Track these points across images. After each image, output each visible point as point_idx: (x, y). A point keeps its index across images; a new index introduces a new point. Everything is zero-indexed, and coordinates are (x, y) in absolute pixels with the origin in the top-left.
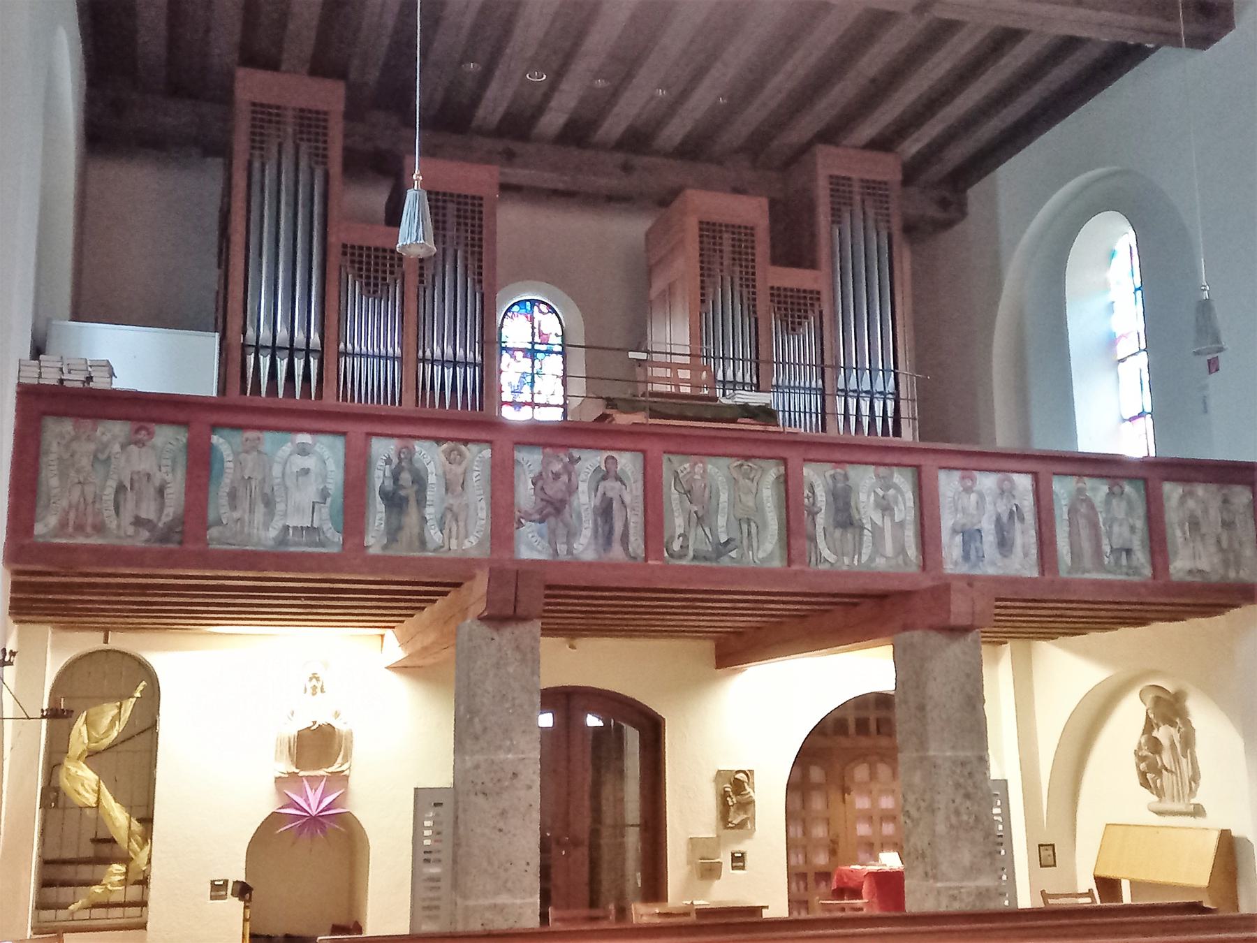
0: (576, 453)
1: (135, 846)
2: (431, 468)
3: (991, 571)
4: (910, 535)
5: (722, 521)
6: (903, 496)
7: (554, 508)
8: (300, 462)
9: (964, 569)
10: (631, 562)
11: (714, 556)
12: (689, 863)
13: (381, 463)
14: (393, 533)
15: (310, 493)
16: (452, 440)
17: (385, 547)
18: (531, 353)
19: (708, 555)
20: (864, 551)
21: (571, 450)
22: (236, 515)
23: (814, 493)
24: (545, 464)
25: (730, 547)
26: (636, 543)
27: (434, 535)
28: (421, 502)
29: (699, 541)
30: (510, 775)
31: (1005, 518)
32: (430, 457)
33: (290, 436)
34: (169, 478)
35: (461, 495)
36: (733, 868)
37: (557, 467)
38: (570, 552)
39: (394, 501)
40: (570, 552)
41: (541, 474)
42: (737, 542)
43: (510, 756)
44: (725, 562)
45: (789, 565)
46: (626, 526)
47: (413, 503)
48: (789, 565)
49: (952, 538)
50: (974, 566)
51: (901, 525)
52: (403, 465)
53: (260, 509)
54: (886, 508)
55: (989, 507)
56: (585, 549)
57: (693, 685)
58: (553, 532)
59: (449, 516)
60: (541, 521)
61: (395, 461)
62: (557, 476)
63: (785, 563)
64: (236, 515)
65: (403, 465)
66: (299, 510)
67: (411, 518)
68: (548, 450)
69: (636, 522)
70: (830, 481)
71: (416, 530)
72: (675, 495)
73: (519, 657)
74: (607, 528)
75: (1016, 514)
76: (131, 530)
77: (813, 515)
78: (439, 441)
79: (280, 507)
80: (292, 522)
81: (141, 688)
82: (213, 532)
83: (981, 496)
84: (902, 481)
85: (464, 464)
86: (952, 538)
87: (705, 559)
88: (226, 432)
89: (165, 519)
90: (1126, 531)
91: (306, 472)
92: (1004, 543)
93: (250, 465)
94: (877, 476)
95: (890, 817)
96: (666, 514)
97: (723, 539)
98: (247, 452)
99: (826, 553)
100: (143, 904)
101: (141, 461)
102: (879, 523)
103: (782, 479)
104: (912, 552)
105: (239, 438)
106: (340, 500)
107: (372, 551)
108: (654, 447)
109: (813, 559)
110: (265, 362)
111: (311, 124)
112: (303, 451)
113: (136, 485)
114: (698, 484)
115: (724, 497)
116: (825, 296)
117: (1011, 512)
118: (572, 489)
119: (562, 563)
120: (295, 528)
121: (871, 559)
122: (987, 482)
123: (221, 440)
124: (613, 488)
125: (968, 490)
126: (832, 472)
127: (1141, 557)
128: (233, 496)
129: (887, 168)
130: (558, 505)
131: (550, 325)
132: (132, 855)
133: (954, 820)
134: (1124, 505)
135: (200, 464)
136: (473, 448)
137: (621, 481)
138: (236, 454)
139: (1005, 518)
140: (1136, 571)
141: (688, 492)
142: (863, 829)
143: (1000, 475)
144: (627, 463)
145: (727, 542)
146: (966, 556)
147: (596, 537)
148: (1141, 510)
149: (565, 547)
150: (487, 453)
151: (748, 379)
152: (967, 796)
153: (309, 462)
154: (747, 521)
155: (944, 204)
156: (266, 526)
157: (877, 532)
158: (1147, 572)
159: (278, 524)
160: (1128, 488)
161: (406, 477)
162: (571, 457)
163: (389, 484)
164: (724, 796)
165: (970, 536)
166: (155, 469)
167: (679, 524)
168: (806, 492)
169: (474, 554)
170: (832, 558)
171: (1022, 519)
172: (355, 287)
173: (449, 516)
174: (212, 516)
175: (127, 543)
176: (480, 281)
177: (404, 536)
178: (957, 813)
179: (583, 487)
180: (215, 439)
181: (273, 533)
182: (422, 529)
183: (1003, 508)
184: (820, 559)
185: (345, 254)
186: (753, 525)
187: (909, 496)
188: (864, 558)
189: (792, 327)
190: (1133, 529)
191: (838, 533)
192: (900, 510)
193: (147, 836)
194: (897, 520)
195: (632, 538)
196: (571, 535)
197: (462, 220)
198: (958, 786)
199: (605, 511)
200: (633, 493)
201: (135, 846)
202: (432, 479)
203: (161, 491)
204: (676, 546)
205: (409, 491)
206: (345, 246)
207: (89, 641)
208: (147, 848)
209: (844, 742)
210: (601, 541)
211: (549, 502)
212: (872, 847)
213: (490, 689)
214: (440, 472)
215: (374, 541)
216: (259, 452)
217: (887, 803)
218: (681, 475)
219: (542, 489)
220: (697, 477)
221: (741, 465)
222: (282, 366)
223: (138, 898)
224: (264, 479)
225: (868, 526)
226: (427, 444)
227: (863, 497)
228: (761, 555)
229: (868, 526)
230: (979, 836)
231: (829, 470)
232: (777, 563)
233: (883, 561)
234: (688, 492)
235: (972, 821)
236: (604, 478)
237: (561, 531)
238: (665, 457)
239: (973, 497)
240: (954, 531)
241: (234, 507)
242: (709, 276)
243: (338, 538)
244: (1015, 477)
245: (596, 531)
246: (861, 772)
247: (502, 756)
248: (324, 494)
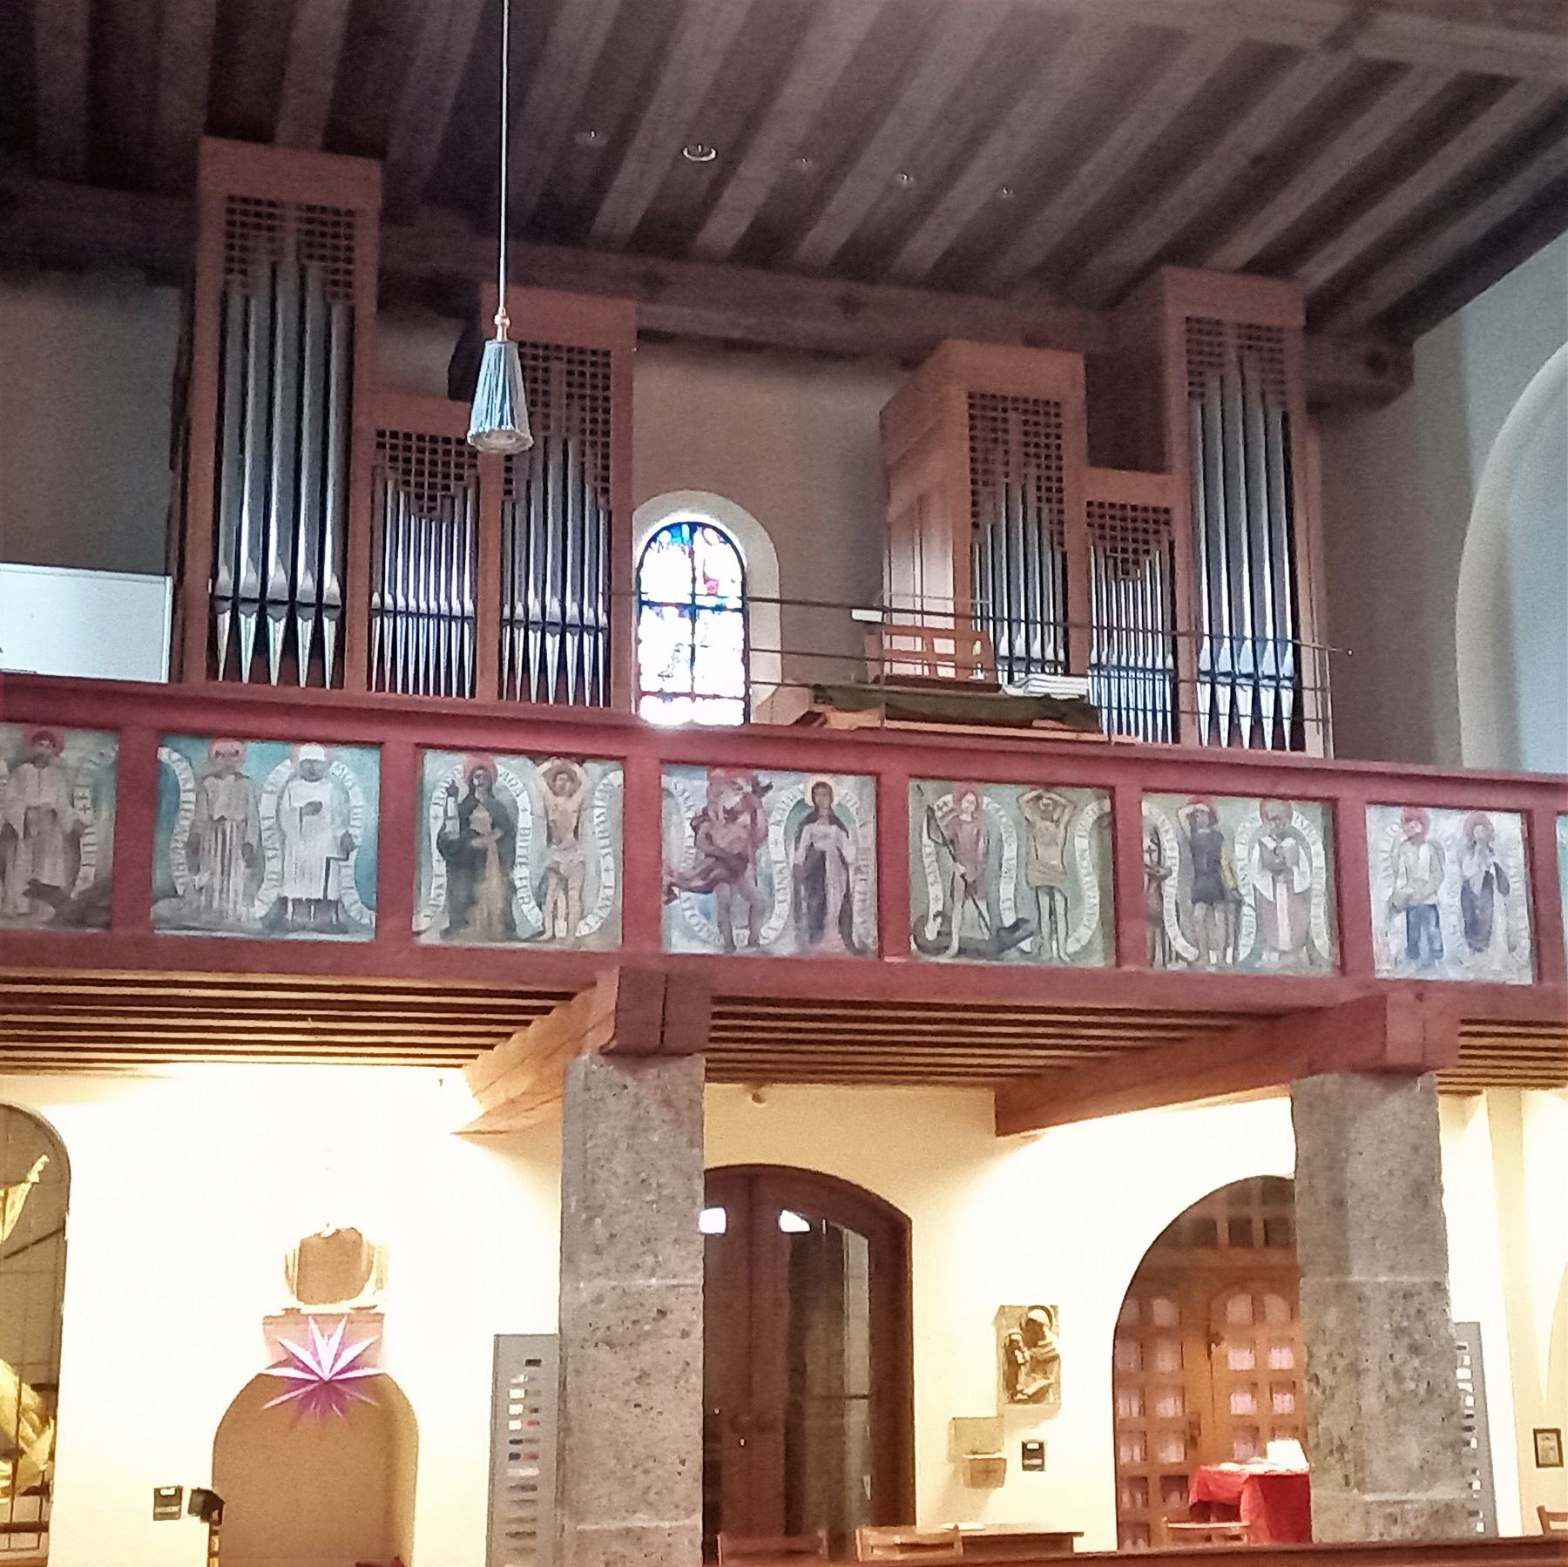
0: (764, 778)
1: (27, 1430)
2: (523, 802)
3: (1453, 974)
4: (1319, 915)
5: (1006, 890)
6: (1307, 848)
7: (727, 868)
9: (1410, 971)
10: (848, 955)
11: (992, 948)
12: (952, 1459)
13: (439, 793)
14: (460, 909)
15: (323, 843)
16: (558, 755)
17: (446, 933)
18: (691, 610)
19: (983, 947)
20: (1242, 942)
21: (755, 772)
22: (202, 879)
23: (1159, 845)
24: (714, 794)
25: (1018, 934)
26: (864, 927)
27: (528, 913)
28: (507, 860)
29: (967, 923)
30: (653, 1314)
31: (1477, 888)
32: (521, 783)
33: (289, 748)
34: (86, 817)
35: (572, 848)
36: (1025, 1468)
37: (732, 800)
38: (753, 942)
39: (463, 858)
40: (753, 942)
41: (705, 811)
42: (1033, 926)
43: (653, 1281)
44: (1012, 958)
45: (1118, 965)
46: (847, 897)
47: (493, 858)
48: (1118, 965)
49: (1390, 918)
50: (1427, 966)
51: (1305, 896)
52: (478, 794)
53: (240, 869)
54: (1278, 869)
55: (1450, 868)
56: (778, 938)
57: (951, 1162)
58: (726, 908)
59: (553, 881)
60: (706, 890)
61: (464, 791)
62: (732, 815)
63: (1113, 961)
64: (202, 879)
65: (478, 794)
66: (303, 872)
68: (719, 772)
69: (863, 888)
70: (1186, 825)
71: (499, 906)
72: (928, 847)
73: (668, 1115)
74: (815, 903)
75: (1494, 880)
76: (24, 905)
77: (1158, 880)
78: (536, 756)
79: (272, 866)
80: (292, 892)
81: (39, 1166)
82: (162, 908)
83: (1437, 850)
84: (1307, 823)
85: (577, 798)
86: (1390, 918)
87: (980, 954)
88: (184, 743)
89: (80, 886)
91: (315, 808)
92: (1476, 930)
93: (222, 798)
94: (1263, 814)
95: (1285, 1383)
96: (915, 882)
97: (1009, 920)
98: (218, 776)
99: (1179, 944)
100: (40, 1527)
101: (41, 790)
102: (1269, 895)
103: (1107, 821)
104: (1323, 942)
105: (203, 751)
106: (372, 854)
107: (424, 940)
108: (894, 767)
109: (1159, 955)
110: (249, 625)
111: (326, 232)
112: (311, 773)
113: (33, 831)
114: (967, 828)
115: (1010, 852)
116: (1179, 516)
117: (1488, 878)
118: (757, 837)
119: (740, 959)
120: (297, 902)
121: (1255, 954)
122: (1447, 826)
123: (176, 756)
124: (826, 836)
125: (1415, 839)
126: (1189, 809)
128: (194, 847)
129: (1279, 304)
130: (734, 863)
131: (721, 564)
132: (22, 1444)
133: (1392, 1388)
135: (140, 797)
136: (593, 768)
137: (841, 826)
138: (200, 780)
139: (1477, 888)
141: (951, 842)
142: (1242, 1404)
143: (1468, 815)
144: (849, 793)
145: (1016, 926)
146: (1413, 950)
147: (797, 919)
149: (747, 932)
150: (616, 777)
151: (1050, 655)
152: (1415, 1349)
153: (320, 792)
154: (1048, 890)
155: (1375, 364)
156: (250, 898)
157: (1264, 909)
159: (269, 894)
161: (481, 816)
162: (756, 784)
163: (453, 827)
164: (1010, 1348)
165: (1419, 916)
166: (65, 801)
167: (935, 895)
168: (1147, 842)
169: (594, 946)
170: (1190, 953)
171: (1505, 890)
172: (396, 501)
173: (553, 881)
174: (159, 879)
175: (19, 925)
176: (606, 491)
177: (478, 914)
178: (1398, 1376)
179: (776, 833)
180: (164, 754)
181: (260, 910)
182: (509, 903)
183: (1473, 869)
184: (1171, 955)
185: (381, 446)
186: (1058, 896)
187: (1318, 848)
188: (1242, 955)
189: (1123, 567)
191: (1200, 910)
192: (1302, 874)
193: (48, 1414)
194: (1297, 890)
195: (857, 920)
196: (756, 913)
197: (575, 390)
198: (1398, 1332)
199: (812, 873)
201: (27, 1430)
202: (524, 821)
203: (74, 839)
204: (931, 931)
205: (487, 841)
206: (381, 434)
208: (49, 1433)
209: (1208, 1258)
210: (805, 923)
211: (719, 858)
212: (1255, 1434)
213: (621, 1170)
214: (540, 811)
215: (429, 920)
216: (238, 776)
217: (1281, 1359)
218: (939, 814)
219: (709, 837)
220: (965, 817)
221: (1039, 798)
222: (277, 630)
223: (32, 1518)
224: (246, 821)
225: (1250, 900)
226: (517, 761)
227: (1240, 851)
228: (1072, 947)
229: (1250, 900)
230: (1434, 1414)
231: (1184, 806)
232: (1097, 961)
233: (1275, 956)
234: (951, 842)
235: (1422, 1391)
236: (811, 819)
237: (740, 905)
238: (912, 784)
239: (1425, 851)
240: (1393, 909)
241: (195, 869)
242: (985, 484)
243: (369, 918)
244: (1494, 818)
245: (796, 906)
246: (1238, 1309)
247: (640, 1281)
248: (346, 846)
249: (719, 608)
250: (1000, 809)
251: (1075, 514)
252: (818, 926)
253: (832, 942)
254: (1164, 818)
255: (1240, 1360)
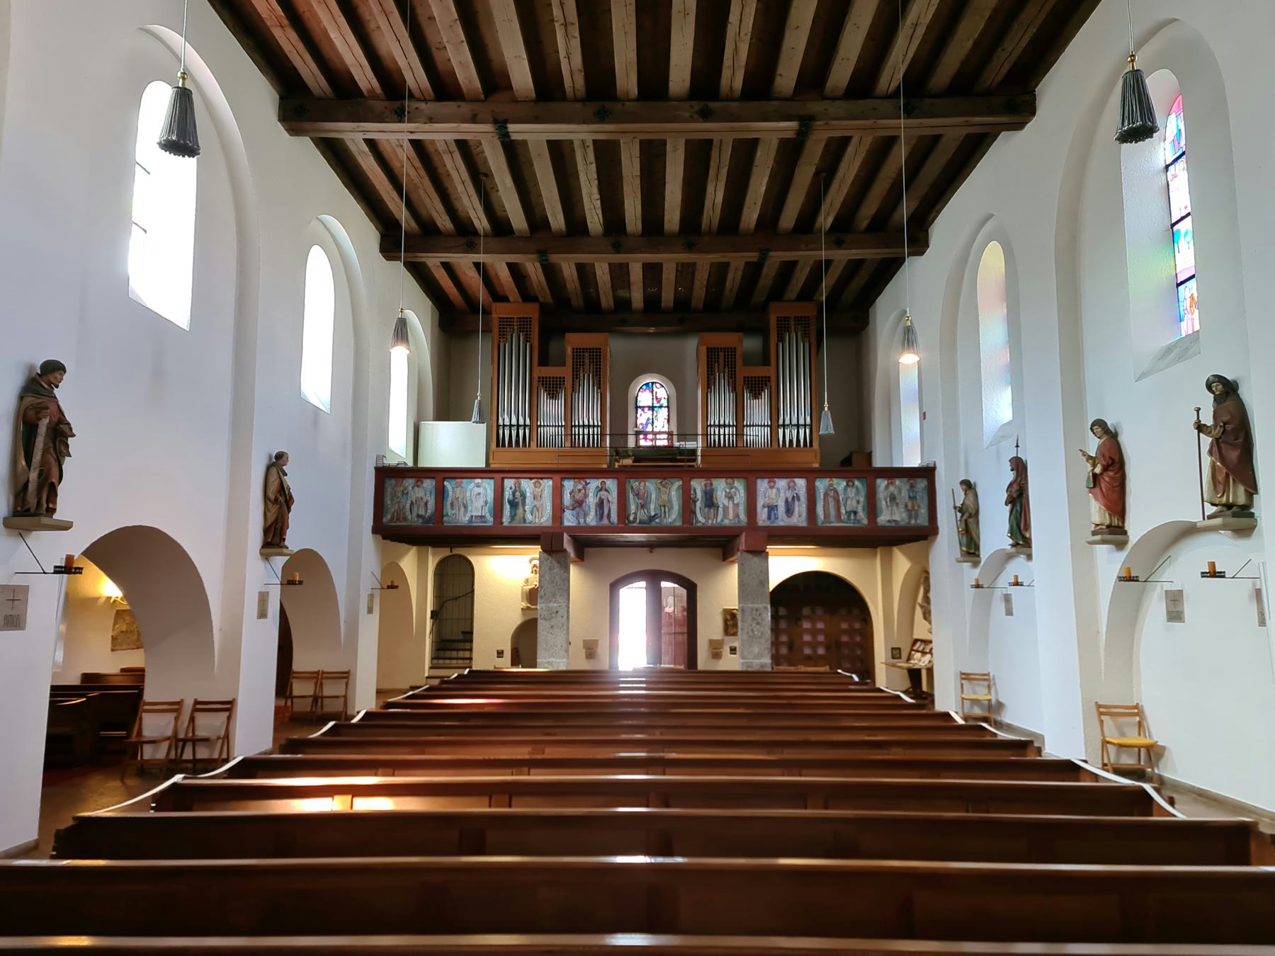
3: (781, 524)
5: (652, 506)
7: (579, 504)
8: (477, 490)
9: (768, 523)
14: (513, 517)
15: (481, 502)
24: (575, 486)
28: (524, 504)
39: (514, 504)
53: (462, 509)
55: (782, 495)
67: (520, 511)
77: (695, 502)
90: (854, 503)
92: (789, 511)
95: (820, 631)
99: (701, 518)
101: (419, 493)
105: (454, 482)
110: (507, 432)
111: (524, 324)
112: (478, 486)
115: (654, 496)
118: (586, 496)
122: (782, 483)
125: (772, 487)
127: (862, 515)
128: (452, 504)
129: (807, 310)
131: (662, 393)
134: (854, 490)
135: (441, 494)
140: (859, 521)
146: (769, 518)
148: (863, 492)
153: (480, 490)
157: (726, 509)
158: (865, 522)
159: (469, 515)
160: (857, 483)
161: (518, 494)
164: (726, 621)
165: (772, 509)
172: (544, 396)
177: (517, 518)
179: (591, 495)
180: (446, 483)
183: (789, 495)
184: (697, 521)
189: (756, 395)
190: (858, 502)
196: (585, 515)
198: (753, 619)
200: (613, 496)
203: (426, 504)
205: (519, 499)
207: (445, 552)
215: (506, 520)
222: (514, 433)
237: (582, 514)
246: (806, 611)
248: (486, 503)
249: (661, 407)
250: (651, 485)
251: (740, 381)
252: (601, 518)
253: (605, 521)
254: (698, 485)
255: (806, 625)
